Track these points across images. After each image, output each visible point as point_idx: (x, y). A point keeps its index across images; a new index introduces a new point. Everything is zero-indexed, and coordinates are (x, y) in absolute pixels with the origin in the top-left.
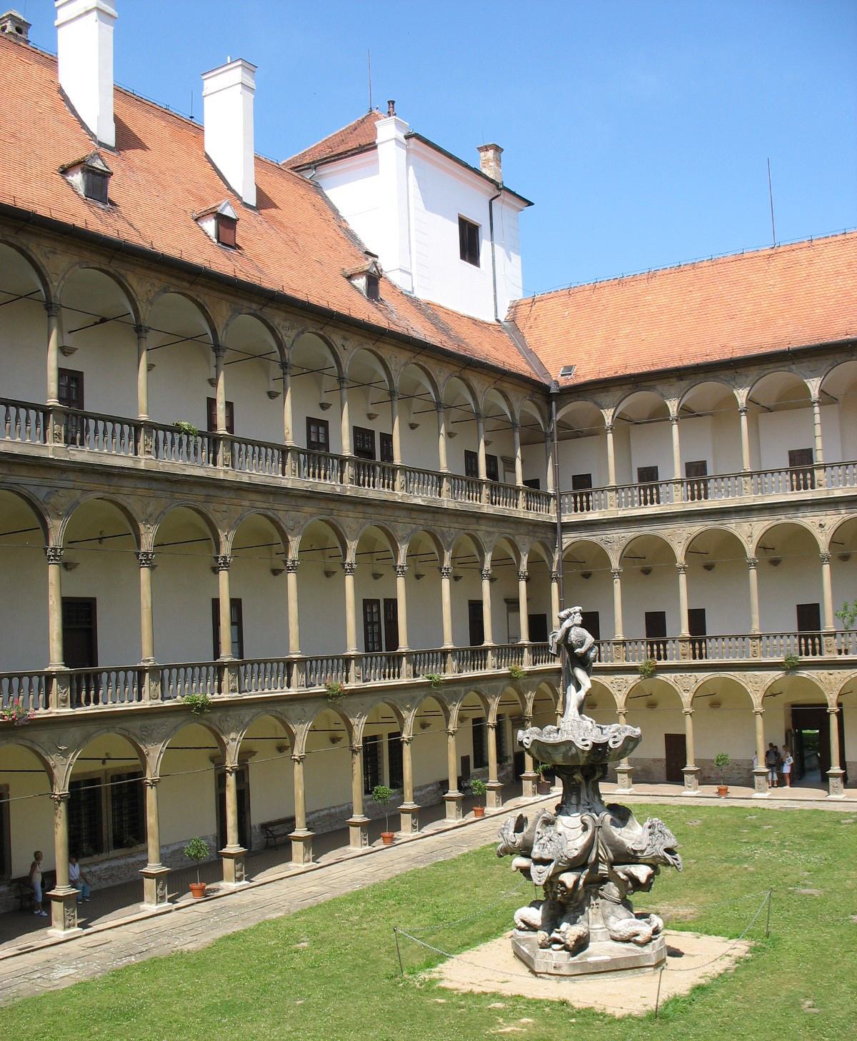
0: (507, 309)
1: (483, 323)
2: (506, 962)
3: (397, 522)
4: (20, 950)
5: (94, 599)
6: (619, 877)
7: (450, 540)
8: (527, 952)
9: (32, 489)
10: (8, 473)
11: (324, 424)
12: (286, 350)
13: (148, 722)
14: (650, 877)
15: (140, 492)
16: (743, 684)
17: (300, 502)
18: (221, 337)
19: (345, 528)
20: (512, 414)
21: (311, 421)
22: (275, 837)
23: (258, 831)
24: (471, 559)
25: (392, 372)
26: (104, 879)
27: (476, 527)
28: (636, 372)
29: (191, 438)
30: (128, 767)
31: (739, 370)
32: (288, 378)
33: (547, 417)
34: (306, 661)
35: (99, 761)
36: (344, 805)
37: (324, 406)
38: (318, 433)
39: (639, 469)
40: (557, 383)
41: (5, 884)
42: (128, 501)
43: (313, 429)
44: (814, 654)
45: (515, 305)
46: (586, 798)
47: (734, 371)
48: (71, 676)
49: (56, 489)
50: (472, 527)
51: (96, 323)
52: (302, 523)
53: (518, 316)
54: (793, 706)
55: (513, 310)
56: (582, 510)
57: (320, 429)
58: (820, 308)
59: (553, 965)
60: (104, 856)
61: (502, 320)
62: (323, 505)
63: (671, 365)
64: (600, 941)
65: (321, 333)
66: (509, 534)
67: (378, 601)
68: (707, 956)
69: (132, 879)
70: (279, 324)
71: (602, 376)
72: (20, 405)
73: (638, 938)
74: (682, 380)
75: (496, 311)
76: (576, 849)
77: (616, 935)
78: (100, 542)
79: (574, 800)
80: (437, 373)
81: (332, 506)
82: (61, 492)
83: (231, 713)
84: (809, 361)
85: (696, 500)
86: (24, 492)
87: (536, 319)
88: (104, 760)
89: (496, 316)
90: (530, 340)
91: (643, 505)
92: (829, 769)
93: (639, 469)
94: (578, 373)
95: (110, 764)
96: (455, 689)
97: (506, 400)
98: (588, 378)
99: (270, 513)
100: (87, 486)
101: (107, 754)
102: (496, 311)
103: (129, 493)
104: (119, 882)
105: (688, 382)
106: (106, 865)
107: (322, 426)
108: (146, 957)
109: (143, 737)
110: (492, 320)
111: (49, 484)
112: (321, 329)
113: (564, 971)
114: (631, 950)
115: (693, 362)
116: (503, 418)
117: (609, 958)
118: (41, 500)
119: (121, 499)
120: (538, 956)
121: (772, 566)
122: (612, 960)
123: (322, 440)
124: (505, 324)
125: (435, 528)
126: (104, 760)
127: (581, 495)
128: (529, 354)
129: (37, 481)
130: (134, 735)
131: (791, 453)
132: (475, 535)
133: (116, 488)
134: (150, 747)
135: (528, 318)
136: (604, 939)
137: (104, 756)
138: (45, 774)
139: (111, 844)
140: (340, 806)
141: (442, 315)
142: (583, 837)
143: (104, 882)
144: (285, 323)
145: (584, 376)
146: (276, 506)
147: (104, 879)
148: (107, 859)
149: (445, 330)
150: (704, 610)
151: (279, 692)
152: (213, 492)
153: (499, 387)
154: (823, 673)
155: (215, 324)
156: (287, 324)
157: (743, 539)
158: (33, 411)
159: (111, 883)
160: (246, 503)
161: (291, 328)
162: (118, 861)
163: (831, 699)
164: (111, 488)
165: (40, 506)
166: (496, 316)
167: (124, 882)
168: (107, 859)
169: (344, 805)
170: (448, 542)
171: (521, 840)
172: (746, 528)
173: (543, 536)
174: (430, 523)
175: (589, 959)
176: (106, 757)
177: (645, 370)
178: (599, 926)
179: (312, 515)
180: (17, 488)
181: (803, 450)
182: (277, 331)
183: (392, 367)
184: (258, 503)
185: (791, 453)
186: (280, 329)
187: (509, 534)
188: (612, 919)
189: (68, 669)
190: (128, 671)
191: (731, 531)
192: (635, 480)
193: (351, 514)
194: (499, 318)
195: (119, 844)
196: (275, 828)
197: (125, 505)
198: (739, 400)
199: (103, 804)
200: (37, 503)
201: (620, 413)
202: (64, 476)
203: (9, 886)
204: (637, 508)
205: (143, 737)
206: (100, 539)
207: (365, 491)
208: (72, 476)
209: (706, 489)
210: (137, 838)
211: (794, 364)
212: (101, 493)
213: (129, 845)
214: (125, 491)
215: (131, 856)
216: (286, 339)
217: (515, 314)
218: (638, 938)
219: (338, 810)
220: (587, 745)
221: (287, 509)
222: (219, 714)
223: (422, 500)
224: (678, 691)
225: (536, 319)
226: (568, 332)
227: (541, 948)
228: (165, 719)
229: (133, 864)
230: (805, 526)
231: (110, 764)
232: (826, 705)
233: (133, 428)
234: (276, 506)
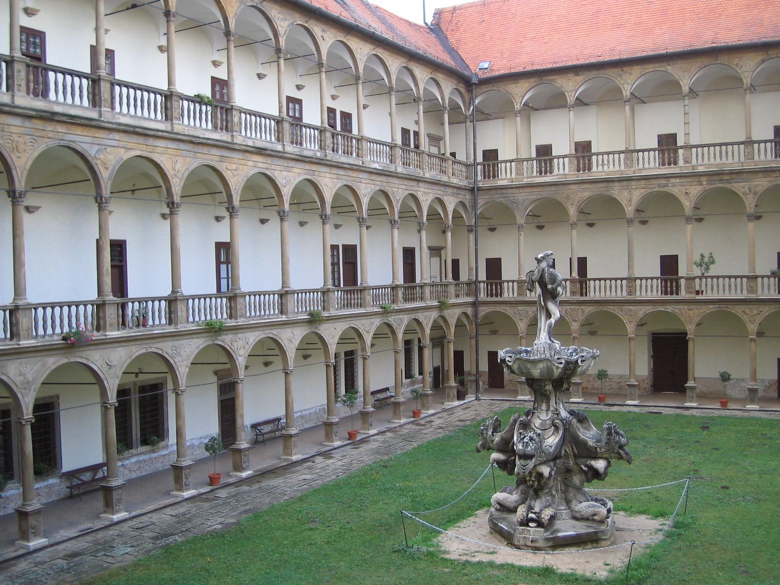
0: (432, 15)
1: (416, 25)
2: (485, 536)
3: (360, 182)
4: (81, 531)
5: (125, 241)
6: (582, 469)
7: (398, 198)
8: (506, 528)
9: (85, 146)
10: (67, 132)
11: (299, 102)
12: (280, 38)
13: (177, 343)
14: (606, 468)
15: (170, 151)
16: (620, 316)
17: (291, 164)
18: (232, 24)
19: (323, 187)
20: (443, 98)
21: (290, 99)
22: (263, 435)
23: (249, 429)
24: (412, 214)
25: (358, 60)
26: (134, 471)
27: (417, 189)
28: (542, 68)
29: (204, 108)
30: (152, 379)
31: (625, 69)
32: (282, 61)
33: (467, 101)
34: (245, 296)
35: (132, 375)
36: (312, 408)
37: (299, 88)
38: (295, 109)
39: (537, 146)
40: (476, 74)
41: (57, 476)
42: (161, 159)
43: (291, 105)
44: (672, 294)
45: (439, 12)
46: (555, 405)
47: (620, 69)
48: (118, 304)
49: (104, 147)
50: (413, 188)
51: (128, 9)
52: (292, 181)
53: (442, 21)
54: (653, 334)
55: (437, 16)
56: (669, 164)
57: (296, 105)
58: (690, 21)
59: (531, 539)
60: (133, 451)
61: (429, 24)
62: (307, 166)
63: (570, 64)
64: (564, 520)
65: (307, 25)
66: (439, 195)
67: (338, 246)
68: (642, 531)
69: (155, 470)
70: (275, 16)
71: (513, 71)
72: (74, 74)
73: (595, 518)
74: (578, 76)
75: (424, 17)
76: (551, 447)
77: (578, 515)
78: (133, 194)
79: (544, 407)
80: (390, 63)
81: (314, 167)
82: (109, 150)
83: (239, 335)
84: (682, 63)
85: (587, 171)
86: (79, 148)
87: (456, 24)
88: (137, 374)
89: (424, 20)
90: (452, 40)
91: (487, 179)
92: (687, 383)
93: (537, 146)
94: (493, 68)
95: (142, 377)
96: (400, 317)
97: (438, 88)
98: (502, 72)
99: (268, 173)
100: (130, 145)
101: (140, 369)
102: (424, 17)
103: (162, 152)
104: (144, 473)
105: (584, 77)
106: (134, 460)
107: (298, 103)
108: (190, 536)
109: (173, 354)
110: (422, 23)
111: (99, 142)
112: (306, 22)
113: (540, 544)
114: (590, 526)
115: (588, 61)
116: (435, 102)
117: (575, 533)
118: (93, 155)
119: (156, 157)
120: (517, 532)
121: (642, 225)
122: (577, 535)
123: (297, 115)
124: (431, 27)
125: (388, 188)
126: (137, 374)
127: (583, 157)
128: (452, 51)
129: (88, 140)
130: (167, 353)
131: (659, 136)
132: (416, 194)
133: (152, 147)
134: (555, 374)
135: (451, 22)
136: (567, 518)
137: (137, 371)
138: (97, 386)
139: (139, 442)
140: (309, 409)
141: (387, 17)
142: (553, 437)
143: (134, 473)
144: (279, 15)
145: (498, 70)
146: (273, 167)
147: (134, 471)
148: (136, 455)
149: (391, 28)
150: (677, 256)
151: (274, 318)
152: (225, 153)
153: (434, 77)
154: (684, 307)
155: (227, 13)
156: (281, 16)
157: (624, 202)
158: (86, 80)
159: (139, 474)
160: (250, 163)
161: (285, 20)
162: (144, 456)
163: (690, 329)
164: (148, 147)
165: (93, 162)
166: (424, 20)
167: (148, 472)
168: (136, 455)
169: (312, 408)
170: (397, 200)
171: (500, 438)
172: (626, 195)
173: (463, 197)
174: (384, 184)
175: (560, 534)
176: (139, 371)
177: (548, 67)
178: (563, 508)
179: (299, 174)
180: (73, 145)
181: (669, 134)
182: (274, 22)
183: (357, 56)
184: (259, 163)
185: (659, 136)
186: (276, 20)
187: (439, 195)
188: (574, 502)
189: (115, 298)
190: (161, 300)
191: (614, 196)
192: (534, 155)
193: (328, 175)
194: (427, 21)
195: (145, 442)
196: (262, 428)
197: (159, 162)
198: (624, 92)
199: (133, 410)
200: (89, 158)
201: (525, 102)
202: (111, 136)
203: (60, 478)
204: (544, 176)
205: (173, 354)
206: (133, 191)
207: (338, 157)
208: (117, 136)
209: (551, 166)
210: (158, 437)
211: (669, 65)
212: (140, 152)
213: (152, 444)
214: (159, 150)
215: (154, 451)
216: (280, 28)
217: (439, 19)
218: (595, 518)
219: (307, 412)
220: (561, 363)
221: (280, 169)
222: (230, 336)
223: (379, 166)
224: (568, 320)
225: (456, 24)
226: (484, 35)
227: (520, 526)
228: (190, 340)
229: (155, 458)
230: (674, 194)
231: (142, 377)
232: (686, 334)
233: (164, 98)
234: (273, 167)
